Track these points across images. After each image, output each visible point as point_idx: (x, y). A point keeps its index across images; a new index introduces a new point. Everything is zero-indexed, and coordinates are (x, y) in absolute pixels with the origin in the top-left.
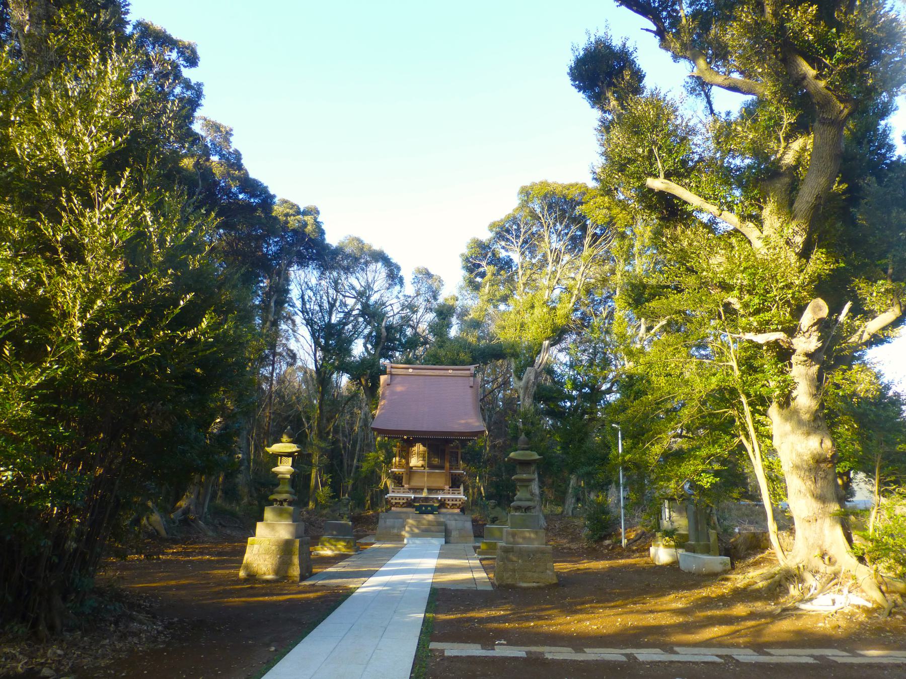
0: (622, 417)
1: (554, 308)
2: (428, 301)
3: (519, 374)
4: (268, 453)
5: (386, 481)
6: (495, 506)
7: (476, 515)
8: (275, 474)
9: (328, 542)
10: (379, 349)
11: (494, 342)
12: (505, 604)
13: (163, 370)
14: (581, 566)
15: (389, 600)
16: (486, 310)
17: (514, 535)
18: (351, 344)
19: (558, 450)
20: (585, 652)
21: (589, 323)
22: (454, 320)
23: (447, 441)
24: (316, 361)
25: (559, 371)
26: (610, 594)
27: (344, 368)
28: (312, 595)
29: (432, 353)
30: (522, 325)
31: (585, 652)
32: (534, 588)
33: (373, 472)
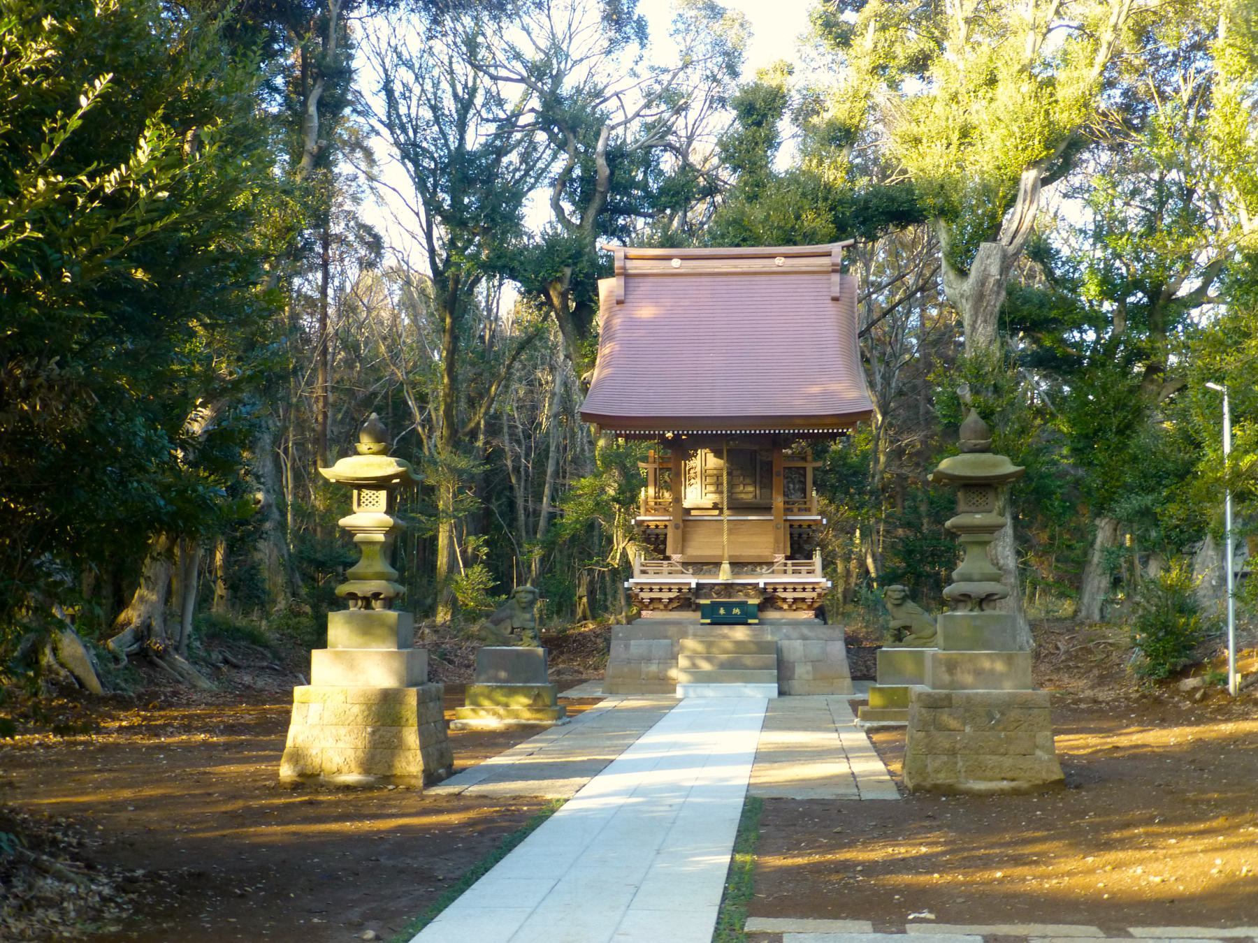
0: (1230, 362)
1: (1050, 82)
2: (715, 79)
3: (960, 262)
4: (326, 481)
5: (627, 549)
6: (904, 599)
7: (857, 626)
8: (348, 533)
9: (489, 697)
10: (591, 213)
11: (895, 178)
12: (931, 829)
13: (52, 275)
14: (1123, 741)
15: (647, 828)
16: (868, 96)
17: (951, 667)
18: (519, 204)
19: (1063, 457)
20: (1130, 936)
21: (1143, 118)
22: (785, 126)
23: (778, 442)
24: (432, 251)
25: (1065, 252)
26: (1195, 803)
27: (504, 265)
28: (455, 818)
29: (730, 216)
30: (965, 133)
31: (1130, 936)
32: (1002, 792)
33: (591, 526)
